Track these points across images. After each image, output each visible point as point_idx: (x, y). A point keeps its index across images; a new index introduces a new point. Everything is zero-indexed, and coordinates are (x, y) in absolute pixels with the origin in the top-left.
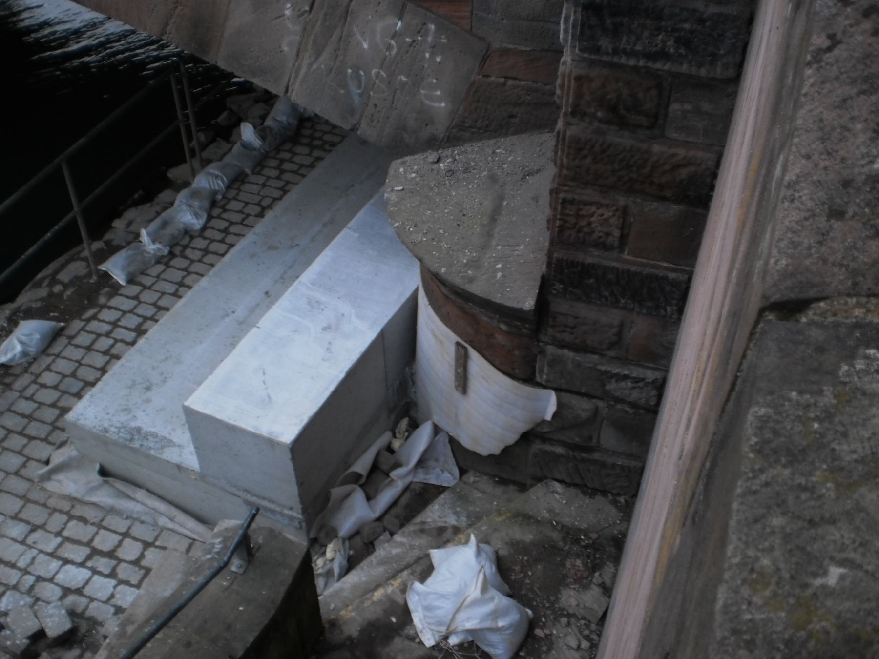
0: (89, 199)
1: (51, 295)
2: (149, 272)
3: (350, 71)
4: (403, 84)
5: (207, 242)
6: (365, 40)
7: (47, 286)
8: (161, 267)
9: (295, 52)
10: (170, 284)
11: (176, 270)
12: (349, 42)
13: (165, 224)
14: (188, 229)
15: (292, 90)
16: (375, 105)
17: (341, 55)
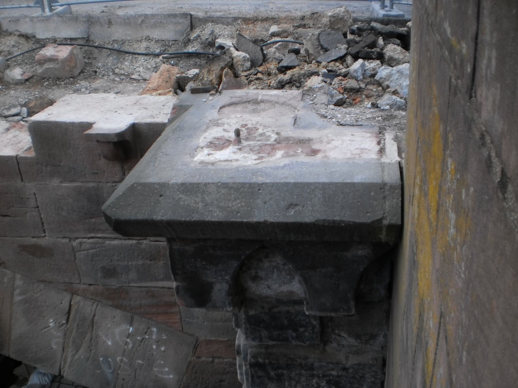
6: (109, 340)
15: (64, 372)
16: (124, 379)
17: (93, 350)
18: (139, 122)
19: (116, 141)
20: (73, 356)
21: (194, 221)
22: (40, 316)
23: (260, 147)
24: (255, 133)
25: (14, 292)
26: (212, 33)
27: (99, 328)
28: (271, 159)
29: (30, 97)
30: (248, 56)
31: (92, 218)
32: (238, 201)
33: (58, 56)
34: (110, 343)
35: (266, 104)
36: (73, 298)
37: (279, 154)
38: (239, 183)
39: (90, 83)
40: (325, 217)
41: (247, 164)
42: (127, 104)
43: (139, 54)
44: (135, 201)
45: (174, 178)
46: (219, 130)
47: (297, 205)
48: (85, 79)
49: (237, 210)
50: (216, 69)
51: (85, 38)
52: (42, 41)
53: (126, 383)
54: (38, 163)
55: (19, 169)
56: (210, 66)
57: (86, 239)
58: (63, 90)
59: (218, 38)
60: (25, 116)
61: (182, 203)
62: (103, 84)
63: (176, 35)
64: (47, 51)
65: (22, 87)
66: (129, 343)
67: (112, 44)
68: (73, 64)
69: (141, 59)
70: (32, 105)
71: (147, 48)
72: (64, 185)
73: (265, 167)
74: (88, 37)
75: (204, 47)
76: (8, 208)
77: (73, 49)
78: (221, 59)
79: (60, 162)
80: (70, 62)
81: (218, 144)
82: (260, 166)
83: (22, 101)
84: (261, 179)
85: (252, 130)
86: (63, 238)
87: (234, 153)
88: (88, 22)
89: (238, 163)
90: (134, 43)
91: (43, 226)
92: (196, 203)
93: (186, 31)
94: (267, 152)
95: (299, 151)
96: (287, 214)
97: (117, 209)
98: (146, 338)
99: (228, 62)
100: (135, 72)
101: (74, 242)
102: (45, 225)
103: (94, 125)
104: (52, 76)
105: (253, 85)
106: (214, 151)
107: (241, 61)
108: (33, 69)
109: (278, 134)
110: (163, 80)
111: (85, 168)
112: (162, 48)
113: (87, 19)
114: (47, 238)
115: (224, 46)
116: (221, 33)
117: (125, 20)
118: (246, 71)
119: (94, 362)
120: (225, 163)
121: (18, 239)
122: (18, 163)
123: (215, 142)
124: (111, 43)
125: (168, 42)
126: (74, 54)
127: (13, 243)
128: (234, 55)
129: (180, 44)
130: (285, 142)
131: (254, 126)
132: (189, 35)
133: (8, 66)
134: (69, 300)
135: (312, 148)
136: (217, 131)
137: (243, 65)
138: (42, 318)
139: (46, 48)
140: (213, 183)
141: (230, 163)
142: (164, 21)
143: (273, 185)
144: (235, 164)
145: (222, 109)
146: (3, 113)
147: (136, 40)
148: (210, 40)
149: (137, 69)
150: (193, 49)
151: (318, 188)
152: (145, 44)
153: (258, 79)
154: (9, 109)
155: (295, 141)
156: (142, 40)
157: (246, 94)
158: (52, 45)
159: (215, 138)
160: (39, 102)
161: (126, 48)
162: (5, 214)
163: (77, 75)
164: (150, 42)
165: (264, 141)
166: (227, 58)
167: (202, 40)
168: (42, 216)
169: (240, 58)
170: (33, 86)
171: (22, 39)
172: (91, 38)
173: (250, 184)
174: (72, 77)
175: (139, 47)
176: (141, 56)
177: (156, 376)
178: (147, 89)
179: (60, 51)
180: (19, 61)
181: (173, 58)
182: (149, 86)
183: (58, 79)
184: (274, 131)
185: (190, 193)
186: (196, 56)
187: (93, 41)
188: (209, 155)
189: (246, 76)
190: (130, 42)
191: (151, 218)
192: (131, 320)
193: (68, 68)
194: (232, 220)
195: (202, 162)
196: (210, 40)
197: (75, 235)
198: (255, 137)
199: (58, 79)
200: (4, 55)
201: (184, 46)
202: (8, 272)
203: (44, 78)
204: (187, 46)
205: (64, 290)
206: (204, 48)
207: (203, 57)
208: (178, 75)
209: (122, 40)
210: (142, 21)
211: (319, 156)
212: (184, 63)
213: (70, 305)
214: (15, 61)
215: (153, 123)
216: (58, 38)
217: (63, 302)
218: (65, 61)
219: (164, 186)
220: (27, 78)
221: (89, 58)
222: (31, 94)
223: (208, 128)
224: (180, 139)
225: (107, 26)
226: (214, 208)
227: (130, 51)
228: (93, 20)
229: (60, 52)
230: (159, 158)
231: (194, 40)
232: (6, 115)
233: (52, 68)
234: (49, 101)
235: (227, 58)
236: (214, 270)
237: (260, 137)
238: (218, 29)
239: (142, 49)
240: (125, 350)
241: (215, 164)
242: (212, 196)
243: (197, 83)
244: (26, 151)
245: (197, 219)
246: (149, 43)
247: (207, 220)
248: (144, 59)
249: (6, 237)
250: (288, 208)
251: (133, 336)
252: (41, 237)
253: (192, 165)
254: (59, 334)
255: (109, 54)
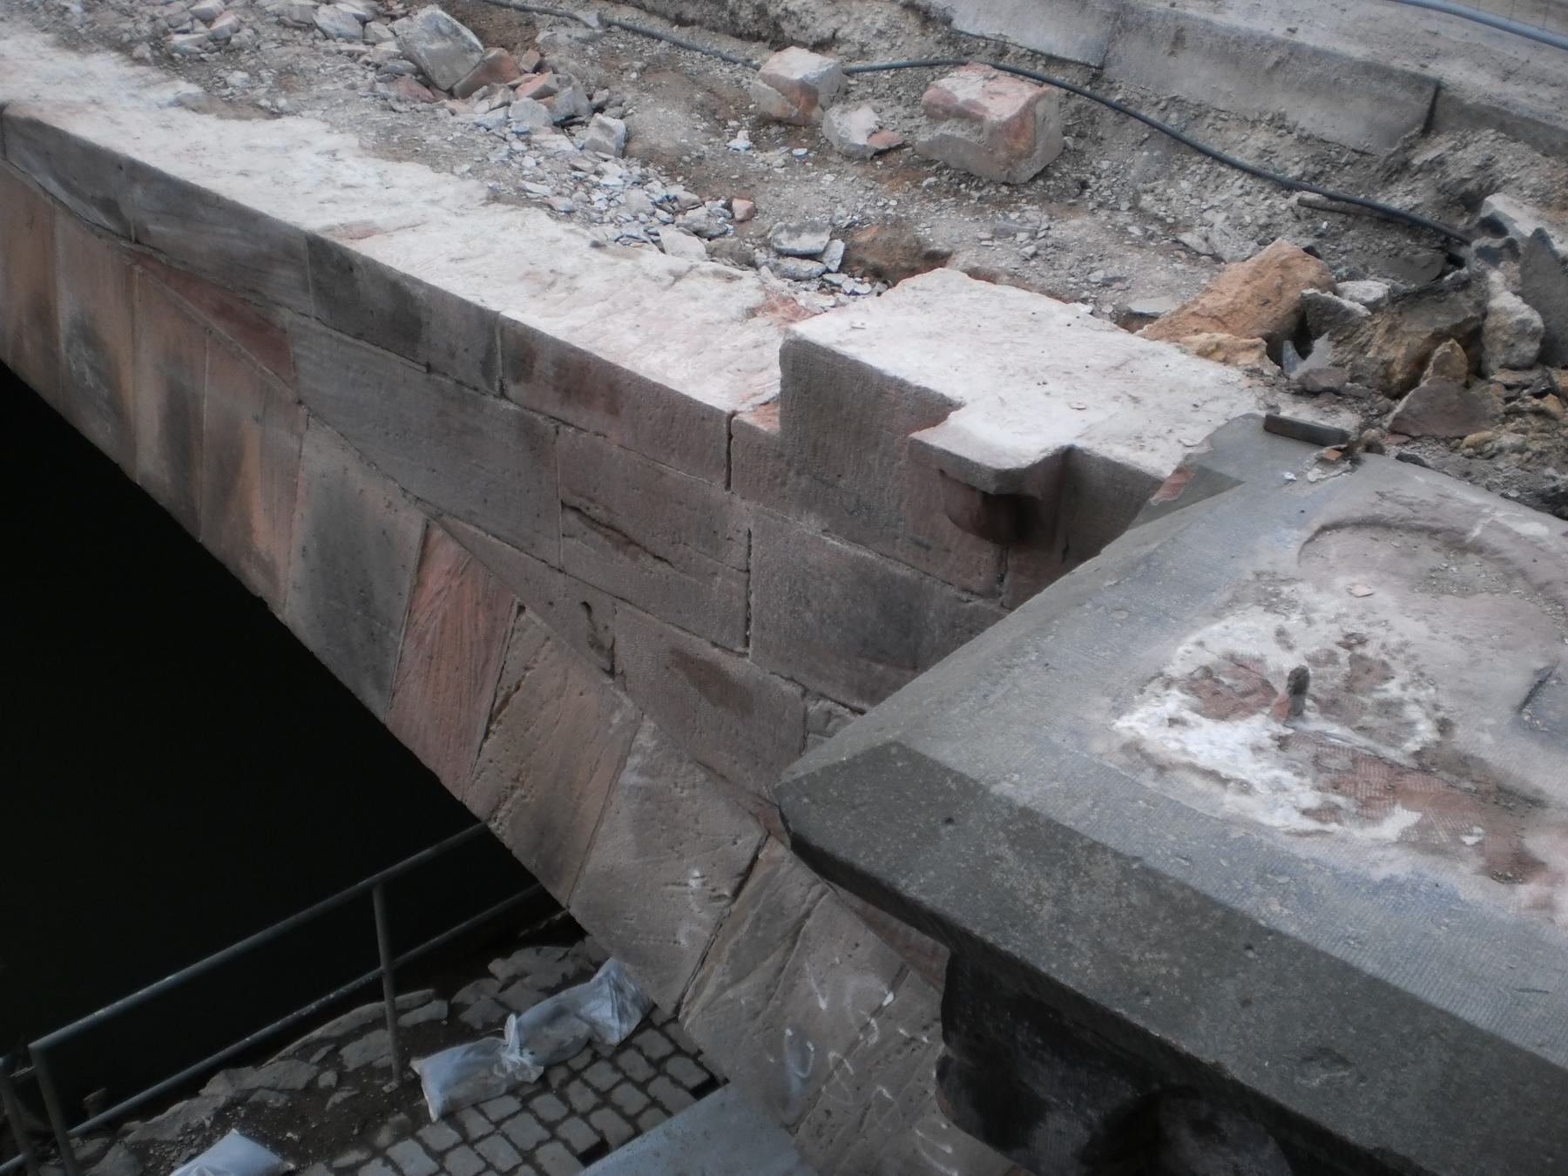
0: (401, 958)
1: (311, 1087)
2: (488, 1107)
3: (789, 1032)
4: (884, 1105)
5: (618, 1077)
6: (824, 996)
7: (318, 1063)
8: (513, 1104)
9: (698, 955)
10: (511, 1149)
11: (533, 1121)
12: (795, 985)
13: (558, 1015)
14: (597, 1038)
15: (687, 1014)
16: (828, 1113)
17: (777, 999)
18: (1088, 450)
19: (991, 493)
20: (722, 988)
21: (1007, 952)
22: (673, 848)
23: (1354, 761)
24: (1372, 690)
25: (629, 758)
26: (1486, 165)
27: (809, 954)
28: (1357, 833)
29: (868, 212)
30: (1537, 321)
31: (879, 661)
32: (1165, 956)
33: (985, 109)
34: (823, 1004)
35: (1487, 567)
36: (768, 845)
37: (1401, 819)
38: (1196, 893)
39: (1051, 219)
40: (1413, 1152)
41: (1266, 820)
42: (1091, 362)
43: (1234, 165)
44: (871, 800)
45: (1016, 777)
46: (1262, 628)
47: (1343, 1061)
48: (1045, 199)
49: (1148, 982)
50: (1418, 332)
51: (1091, 67)
52: (964, 42)
53: (833, 1126)
54: (780, 456)
55: (729, 453)
56: (1400, 313)
57: (847, 710)
58: (967, 219)
59: (1498, 190)
60: (834, 267)
61: (997, 876)
62: (1088, 235)
63: (1370, 136)
64: (962, 82)
65: (860, 170)
66: (873, 1031)
67: (1164, 109)
68: (1021, 146)
69: (1233, 183)
70: (863, 238)
71: (1265, 152)
72: (831, 542)
73: (1315, 861)
74: (1101, 68)
75: (1445, 204)
76: (673, 543)
77: (1039, 98)
78: (1446, 303)
79: (839, 476)
80: (1016, 137)
81: (1229, 687)
82: (1302, 849)
83: (843, 216)
84: (1276, 908)
85: (1369, 671)
86: (787, 679)
87: (1257, 749)
88: (1116, 20)
89: (1244, 800)
90: (1233, 124)
91: (747, 627)
92: (1037, 896)
93: (1406, 132)
94: (1364, 791)
95: (1469, 840)
96: (1298, 1079)
97: (814, 802)
98: (923, 1043)
99: (1468, 321)
100: (1198, 221)
101: (813, 702)
102: (752, 625)
103: (953, 416)
104: (953, 164)
105: (1515, 431)
106: (1196, 711)
107: (1511, 332)
108: (910, 124)
109: (1444, 726)
110: (1256, 291)
111: (900, 520)
112: (1311, 168)
113: (1115, 10)
114: (748, 661)
115: (1507, 224)
116: (1514, 176)
117: (1226, 43)
118: (1514, 368)
119: (769, 1031)
120: (1198, 783)
121: (677, 631)
122: (730, 437)
123: (1223, 673)
124: (1163, 104)
125: (1337, 152)
126: (1035, 115)
127: (661, 636)
128: (1494, 304)
129: (1374, 168)
130: (1446, 776)
131: (1386, 658)
132: (1412, 147)
133: (847, 93)
134: (755, 845)
135: (1523, 845)
136: (1251, 631)
137: (1513, 345)
138: (676, 855)
139: (963, 72)
140: (1117, 855)
141: (1216, 788)
142: (1349, 82)
143: (1301, 951)
144: (1231, 801)
145: (1323, 538)
146: (775, 240)
147: (1241, 117)
148: (1470, 188)
149: (1208, 216)
150: (1408, 199)
151: (1443, 1035)
152: (1264, 139)
153: (1540, 413)
154: (797, 232)
155: (1483, 787)
156: (1261, 122)
157: (1434, 501)
158: (982, 67)
159: (1232, 657)
160: (887, 235)
161: (1202, 134)
162: (660, 555)
163: (1027, 180)
164: (1280, 136)
165: (1379, 741)
166: (1465, 305)
167: (1448, 179)
168: (753, 598)
169: (1509, 322)
170: (891, 177)
171: (912, 19)
172: (1109, 72)
173: (1231, 913)
174: (1005, 184)
175: (1244, 141)
176: (1235, 174)
177: (915, 1151)
178: (1195, 309)
179: (999, 94)
180: (884, 84)
181: (1332, 211)
182: (1202, 301)
183: (969, 177)
184: (1437, 708)
185: (1035, 853)
186: (1409, 227)
187: (1111, 83)
188: (1173, 722)
189: (1508, 387)
190: (1222, 119)
191: (891, 880)
192: (898, 976)
193: (1002, 154)
194: (1118, 1010)
195: (1133, 748)
196: (1471, 186)
197: (821, 686)
198: (1363, 707)
199: (969, 177)
200: (846, 54)
201: (1386, 180)
202: (628, 702)
203: (930, 162)
204: (1392, 183)
205: (750, 813)
206: (1444, 208)
207: (1430, 236)
208: (1311, 291)
209: (1199, 105)
210: (1277, 63)
211: (1527, 892)
212: (1361, 240)
213: (755, 859)
214: (871, 83)
215: (1129, 466)
216: (1015, 45)
217: (739, 842)
218: (1000, 132)
219: (971, 789)
220: (882, 147)
221: (1081, 136)
222: (877, 201)
223: (1234, 602)
224: (1125, 615)
225: (1166, 47)
226: (1083, 941)
227: (1209, 146)
228: (1130, 18)
229: (998, 99)
230: (1017, 671)
231: (1420, 169)
232: (781, 247)
233: (959, 140)
234: (914, 244)
235: (1465, 305)
236: (1060, 1073)
237: (1378, 715)
238: (1510, 157)
239: (1248, 152)
240: (856, 1043)
241: (1168, 775)
242: (1094, 898)
243: (1341, 353)
244: (766, 407)
245: (1017, 953)
246: (1278, 140)
247: (1044, 969)
248: (1242, 187)
249: (647, 612)
250: (1311, 1059)
251: (890, 1018)
252: (732, 651)
253: (1098, 746)
254: (706, 917)
255: (1146, 139)
